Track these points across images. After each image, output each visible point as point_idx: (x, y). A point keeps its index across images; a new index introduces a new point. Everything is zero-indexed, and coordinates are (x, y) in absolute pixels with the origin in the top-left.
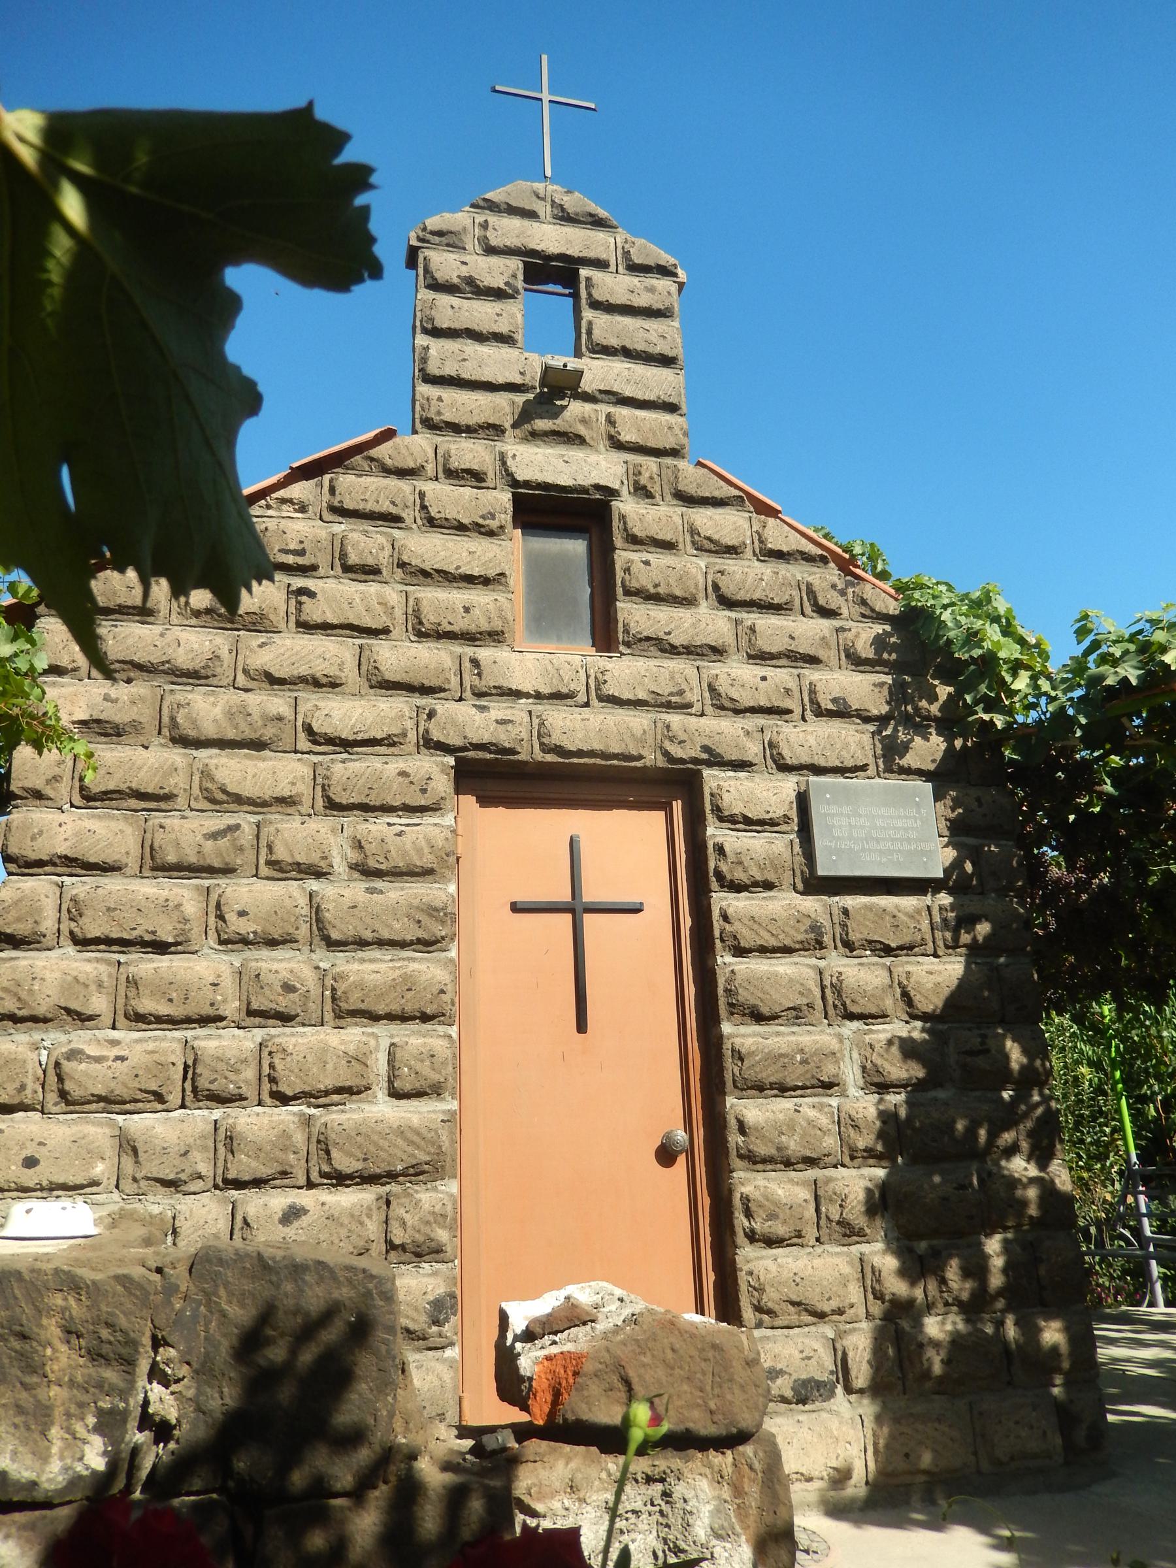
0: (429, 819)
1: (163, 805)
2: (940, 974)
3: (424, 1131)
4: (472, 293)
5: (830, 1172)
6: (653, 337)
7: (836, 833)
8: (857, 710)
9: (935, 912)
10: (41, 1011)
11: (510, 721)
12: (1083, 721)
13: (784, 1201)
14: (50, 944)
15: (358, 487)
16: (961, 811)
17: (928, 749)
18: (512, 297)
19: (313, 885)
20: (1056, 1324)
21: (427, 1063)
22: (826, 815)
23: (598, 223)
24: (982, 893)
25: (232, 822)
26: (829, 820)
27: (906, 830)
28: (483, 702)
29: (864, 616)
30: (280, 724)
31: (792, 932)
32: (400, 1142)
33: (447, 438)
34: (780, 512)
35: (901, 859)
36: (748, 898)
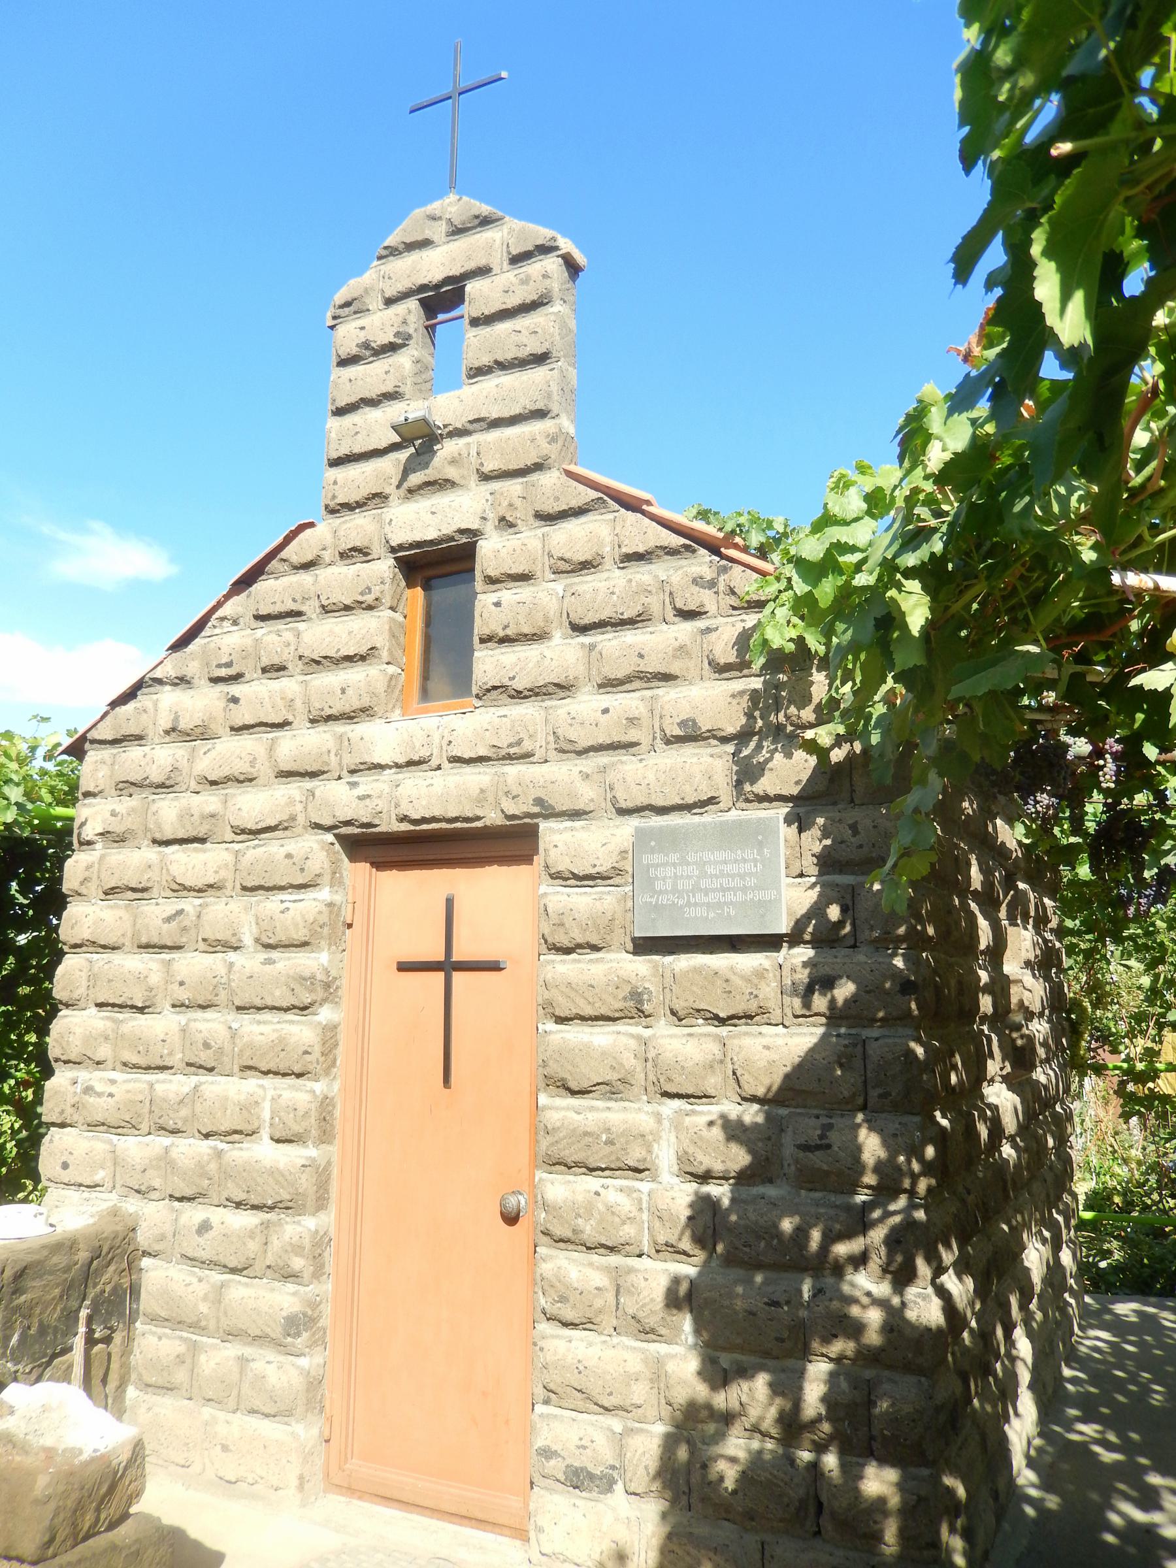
0: (309, 895)
1: (145, 895)
2: (785, 1044)
3: (287, 1173)
4: (373, 355)
5: (633, 1262)
6: (524, 338)
7: (658, 886)
8: (709, 731)
9: (786, 971)
10: (73, 1057)
11: (369, 796)
12: (875, 739)
13: (576, 1285)
14: (83, 1006)
15: (272, 591)
16: (828, 842)
17: (790, 771)
18: (404, 345)
19: (232, 956)
20: (891, 1475)
21: (292, 1115)
22: (648, 866)
23: (485, 222)
24: (854, 946)
25: (179, 907)
26: (652, 871)
27: (742, 877)
28: (355, 778)
29: (734, 608)
30: (213, 820)
31: (610, 1000)
32: (271, 1180)
33: (347, 518)
34: (648, 503)
35: (732, 913)
36: (575, 961)
